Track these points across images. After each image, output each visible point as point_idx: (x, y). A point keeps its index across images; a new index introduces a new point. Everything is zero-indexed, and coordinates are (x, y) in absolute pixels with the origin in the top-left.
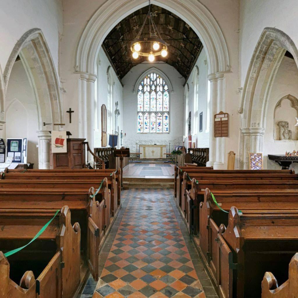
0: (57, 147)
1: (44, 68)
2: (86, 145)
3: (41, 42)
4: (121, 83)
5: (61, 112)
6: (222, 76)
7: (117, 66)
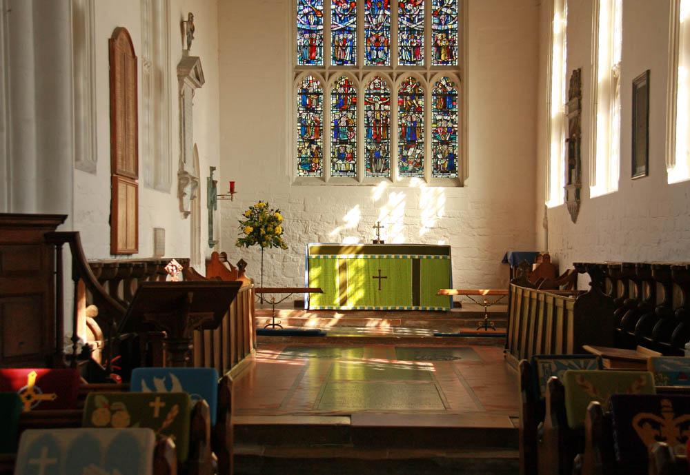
2: (66, 247)
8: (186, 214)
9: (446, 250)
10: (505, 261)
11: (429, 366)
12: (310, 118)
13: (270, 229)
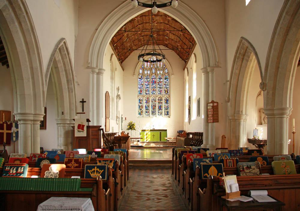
0: (79, 131)
1: (65, 67)
2: (102, 131)
3: (65, 48)
4: (122, 67)
5: (76, 102)
6: (212, 71)
7: (118, 52)
8: (117, 124)
9: (166, 130)
10: (178, 132)
11: (162, 152)
12: (140, 105)
13: (133, 127)
